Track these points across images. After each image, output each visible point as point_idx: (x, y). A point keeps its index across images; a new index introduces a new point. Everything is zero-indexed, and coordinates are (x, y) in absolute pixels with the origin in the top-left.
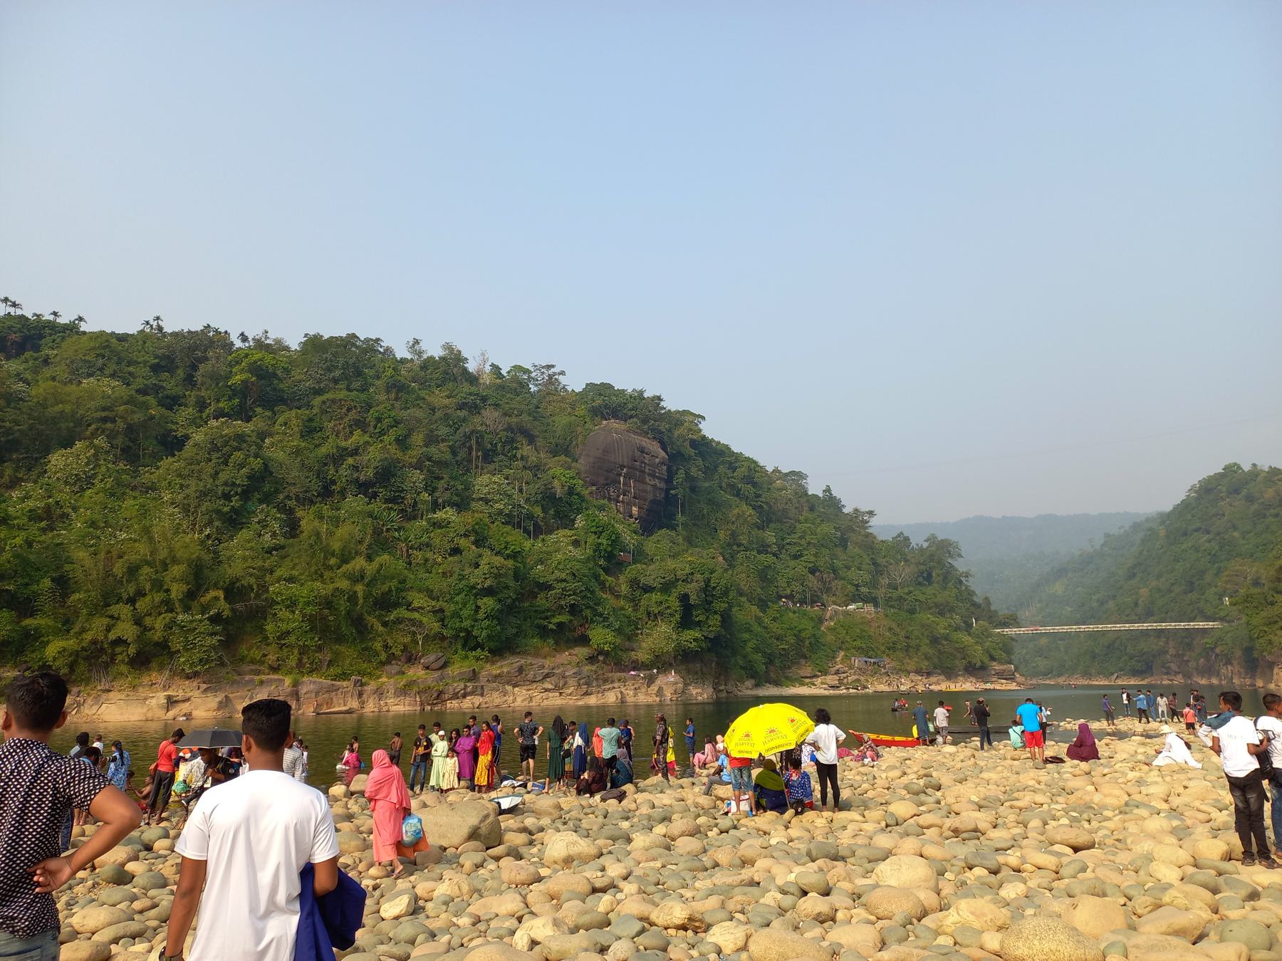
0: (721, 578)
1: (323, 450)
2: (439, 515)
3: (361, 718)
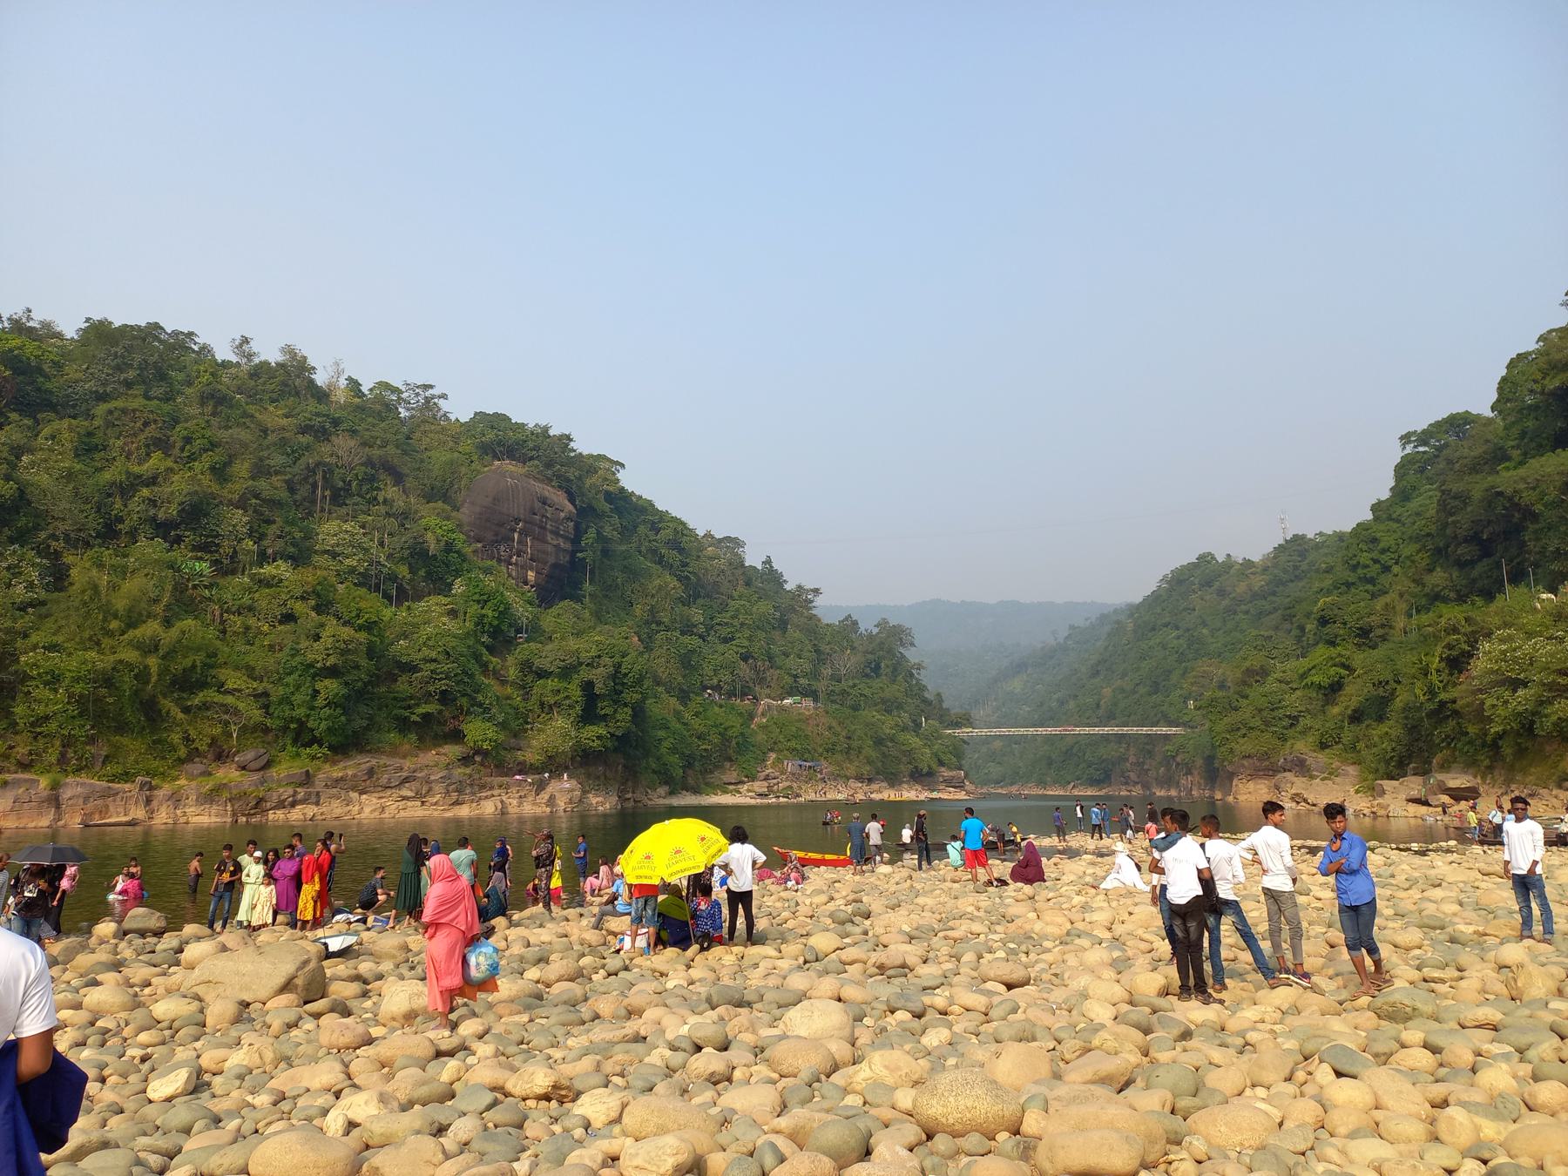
0: (634, 663)
1: (107, 476)
2: (268, 570)
3: (147, 833)
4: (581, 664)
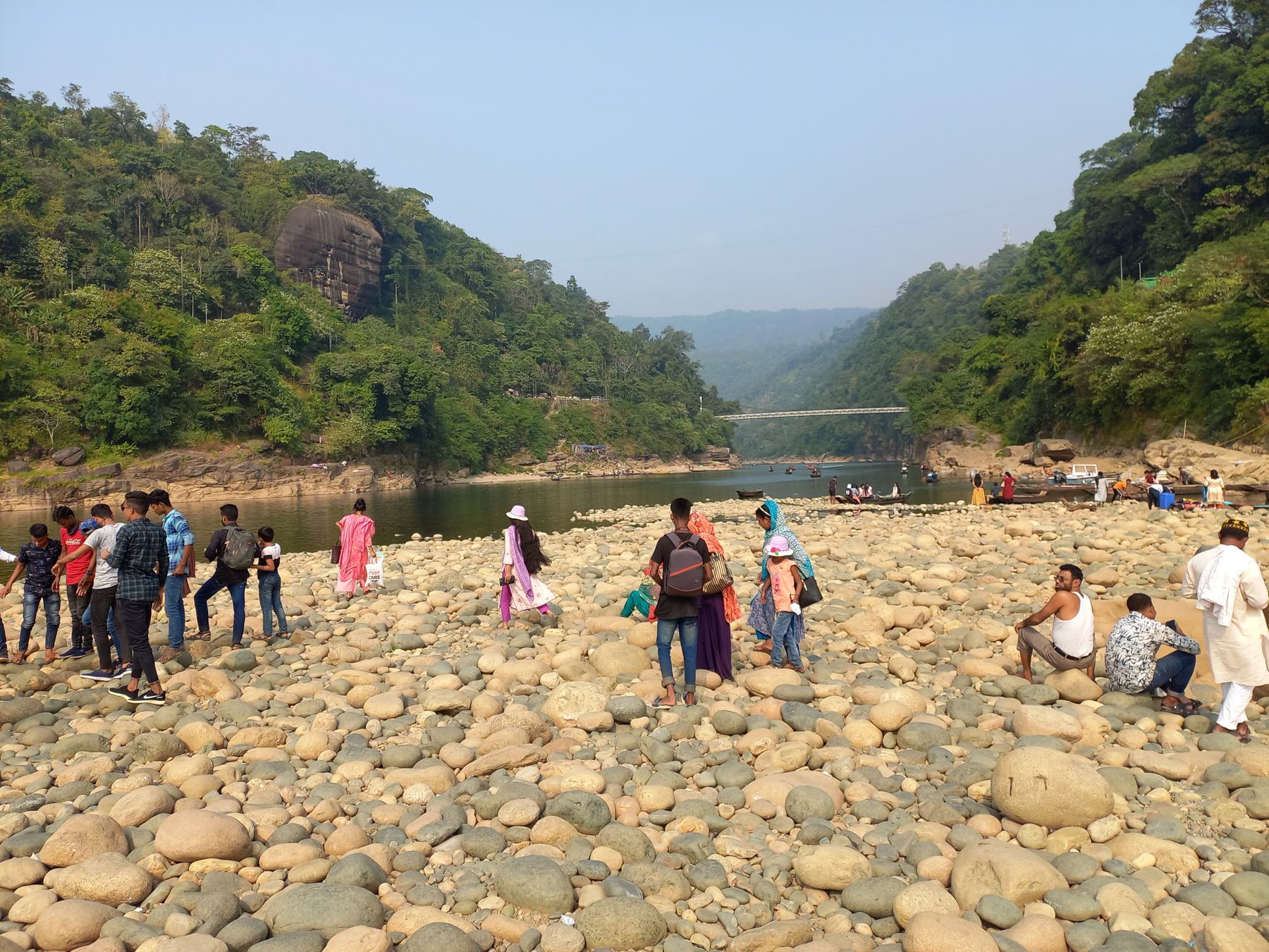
4: (371, 370)
